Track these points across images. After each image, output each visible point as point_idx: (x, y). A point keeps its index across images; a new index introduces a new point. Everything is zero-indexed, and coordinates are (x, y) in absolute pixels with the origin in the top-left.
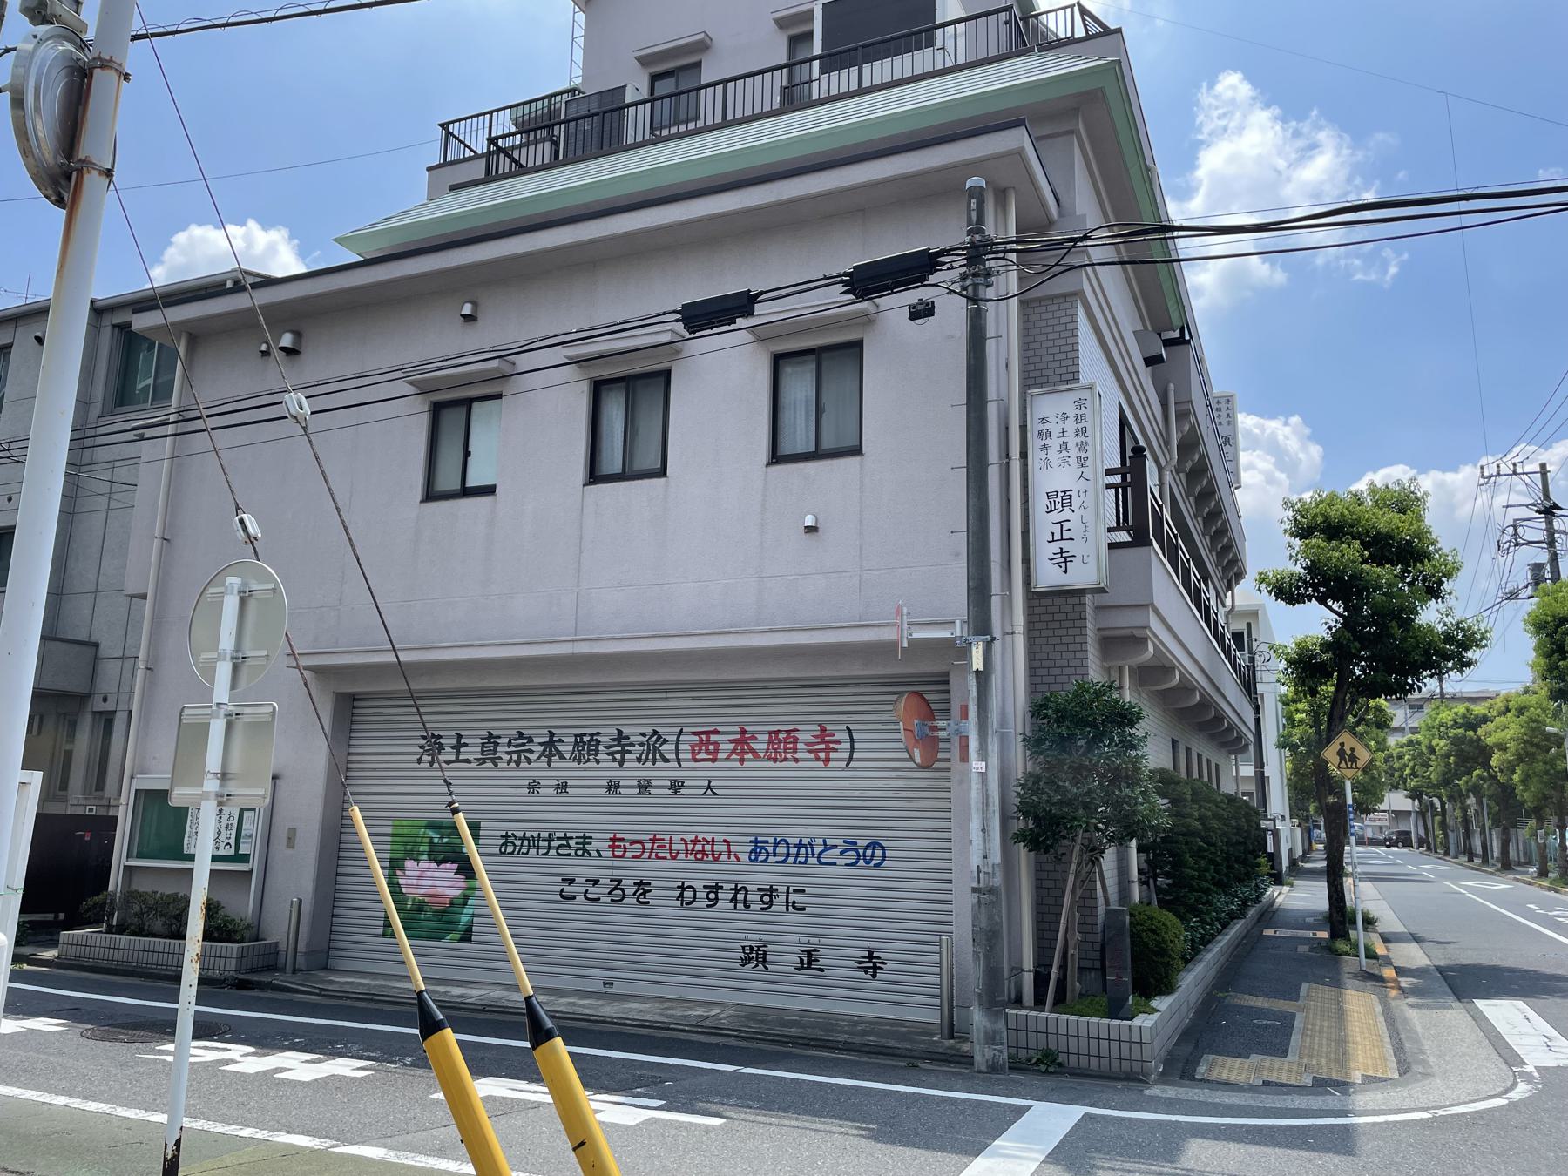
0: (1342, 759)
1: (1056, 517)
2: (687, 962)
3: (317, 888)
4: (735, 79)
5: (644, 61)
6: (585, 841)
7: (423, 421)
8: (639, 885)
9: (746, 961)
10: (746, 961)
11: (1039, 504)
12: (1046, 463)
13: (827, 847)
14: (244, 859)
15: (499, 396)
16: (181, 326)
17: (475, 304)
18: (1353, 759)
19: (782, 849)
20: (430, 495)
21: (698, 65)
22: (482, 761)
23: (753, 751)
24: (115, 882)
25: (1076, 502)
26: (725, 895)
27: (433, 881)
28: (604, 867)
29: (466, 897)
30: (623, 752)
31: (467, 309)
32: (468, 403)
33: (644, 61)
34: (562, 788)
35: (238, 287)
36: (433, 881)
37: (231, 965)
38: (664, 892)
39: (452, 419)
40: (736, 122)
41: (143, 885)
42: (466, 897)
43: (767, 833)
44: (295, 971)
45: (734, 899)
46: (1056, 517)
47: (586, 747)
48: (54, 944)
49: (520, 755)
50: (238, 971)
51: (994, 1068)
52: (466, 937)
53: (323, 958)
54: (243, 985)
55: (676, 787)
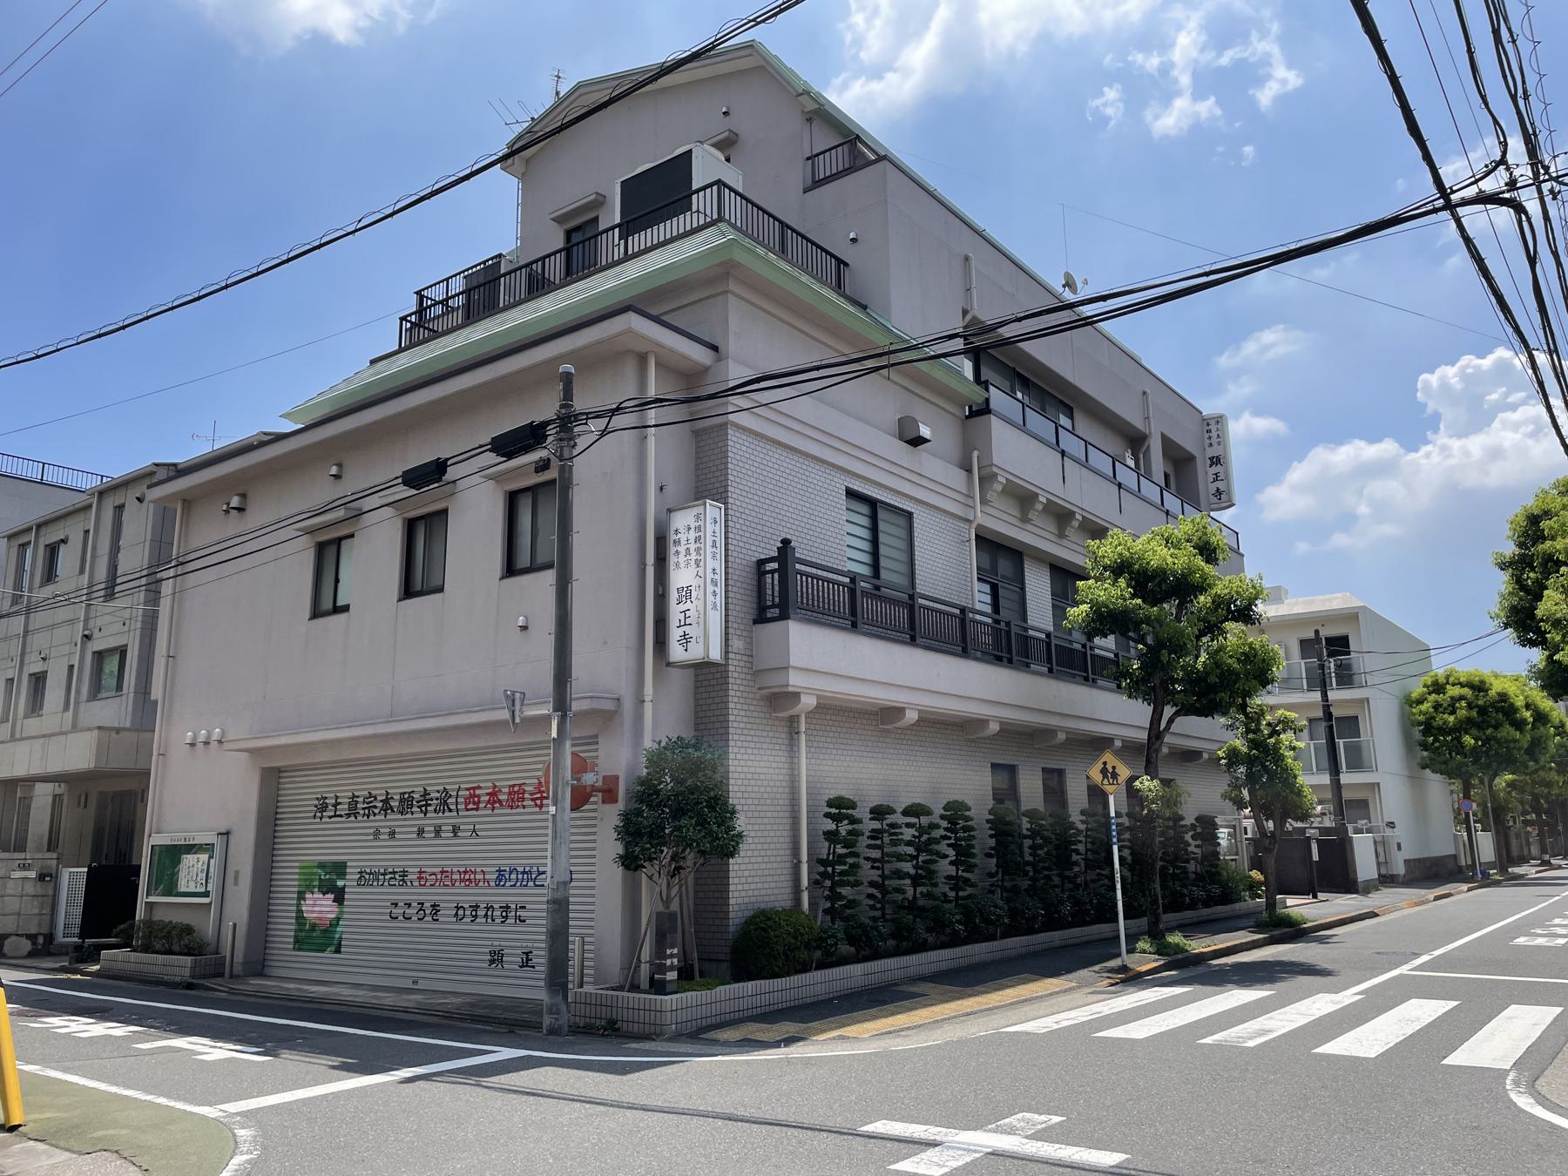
0: (1105, 776)
1: (682, 607)
2: (456, 962)
3: (251, 915)
4: (549, 256)
5: (559, 220)
6: (404, 874)
7: (309, 558)
8: (434, 906)
9: (492, 962)
10: (492, 962)
11: (673, 596)
12: (677, 564)
13: (540, 873)
14: (206, 894)
15: (352, 536)
16: (174, 496)
17: (340, 465)
18: (1115, 775)
19: (513, 876)
20: (316, 613)
21: (596, 219)
22: (349, 815)
23: (500, 802)
24: (140, 913)
25: (694, 594)
26: (481, 913)
27: (320, 907)
28: (414, 893)
29: (338, 919)
30: (427, 805)
31: (334, 470)
32: (338, 541)
33: (559, 220)
34: (392, 834)
35: (262, 444)
36: (320, 907)
37: (187, 972)
38: (447, 913)
39: (332, 550)
40: (636, 255)
41: (159, 915)
42: (338, 919)
43: (506, 864)
44: (231, 976)
45: (486, 916)
46: (682, 607)
47: (406, 803)
48: (97, 961)
49: (370, 811)
50: (193, 977)
51: (553, 1031)
52: (338, 951)
53: (258, 966)
54: (190, 986)
55: (455, 830)
